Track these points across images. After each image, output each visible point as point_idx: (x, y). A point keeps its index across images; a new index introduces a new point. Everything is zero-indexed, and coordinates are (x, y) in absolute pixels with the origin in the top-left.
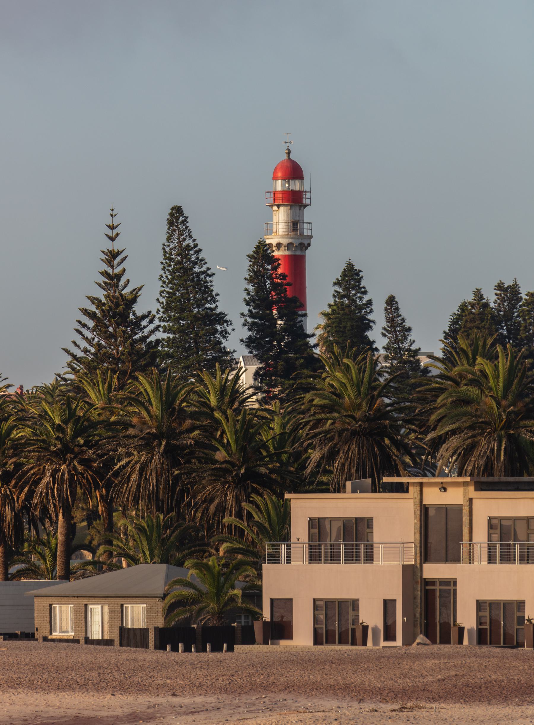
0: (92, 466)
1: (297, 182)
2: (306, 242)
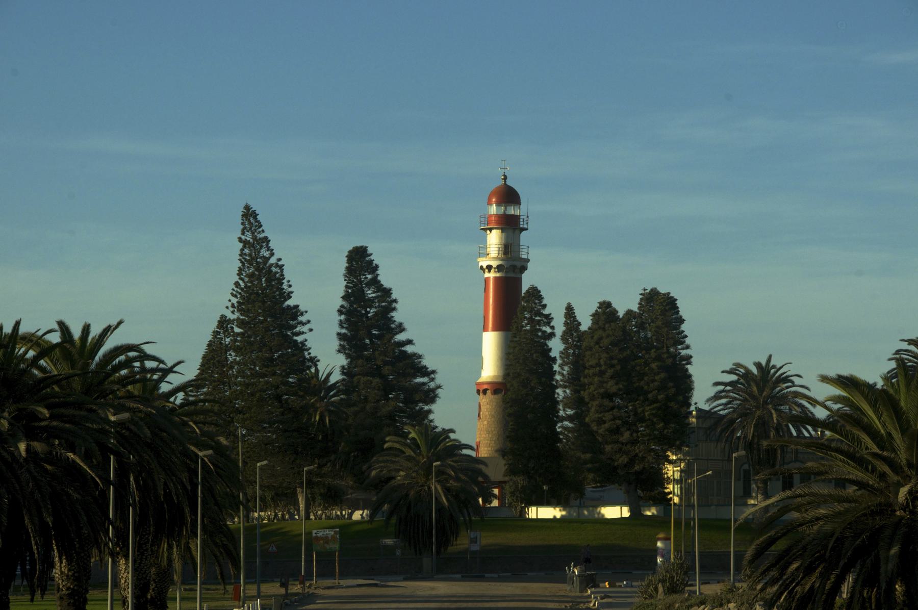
1: (516, 208)
2: (518, 264)
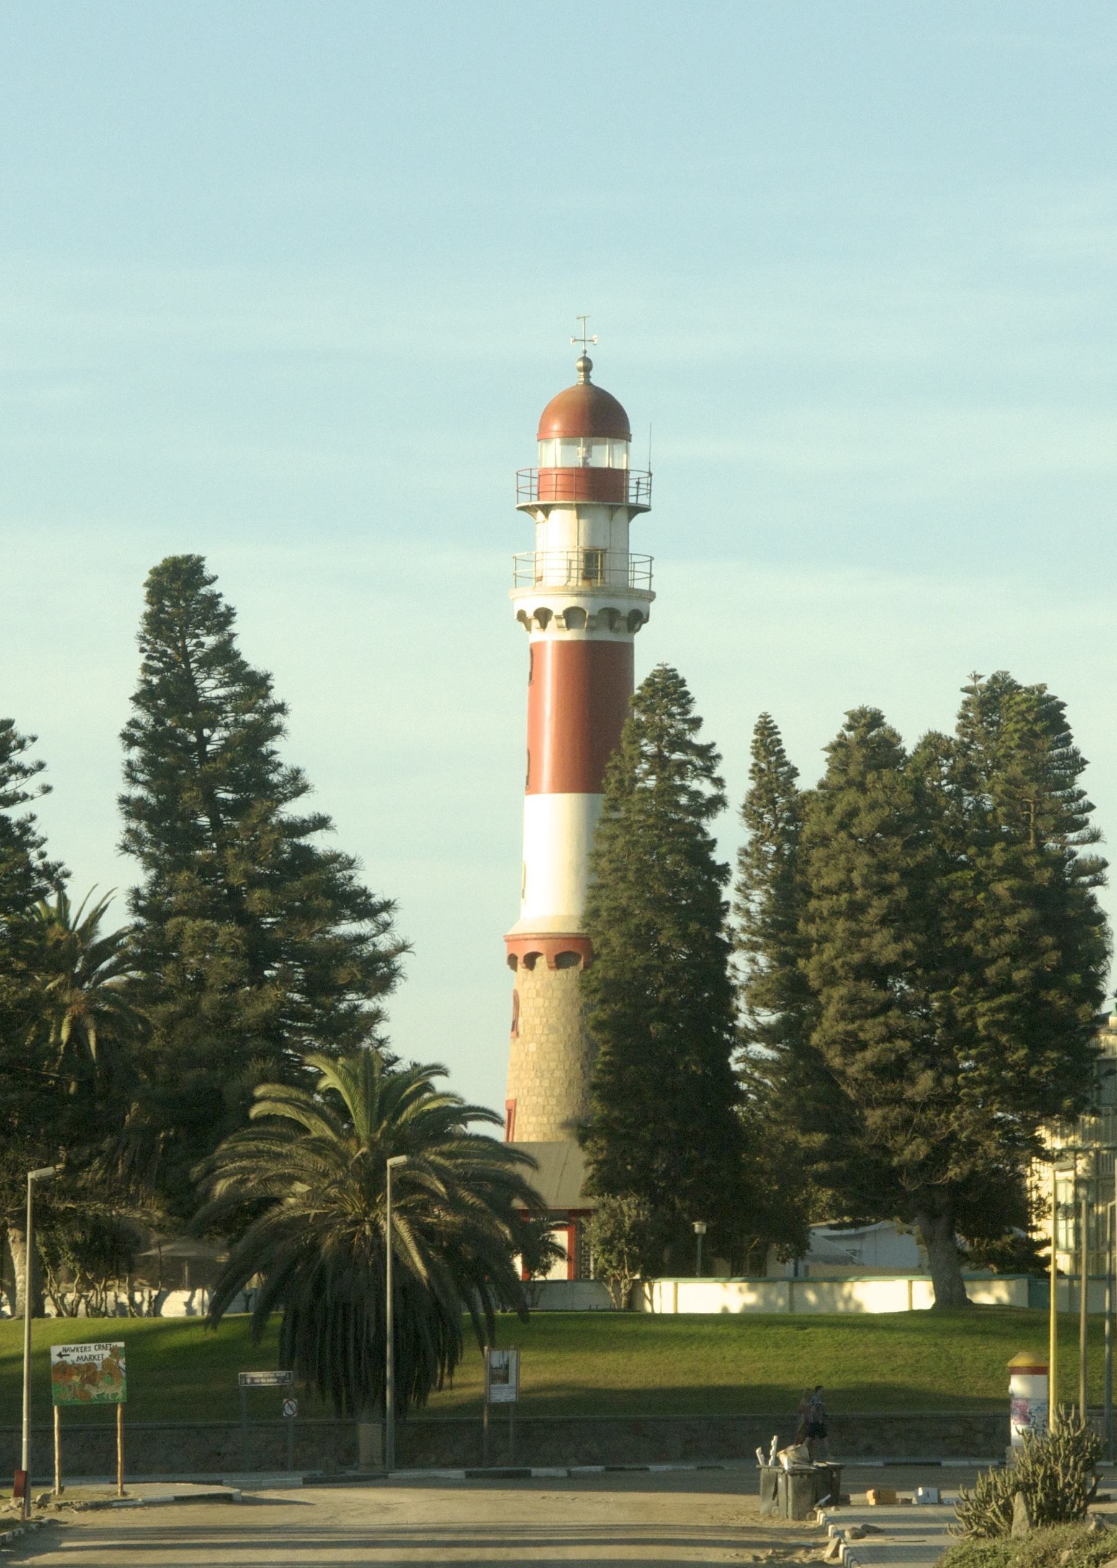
0: (1083, 977)
1: (619, 448)
2: (624, 606)
